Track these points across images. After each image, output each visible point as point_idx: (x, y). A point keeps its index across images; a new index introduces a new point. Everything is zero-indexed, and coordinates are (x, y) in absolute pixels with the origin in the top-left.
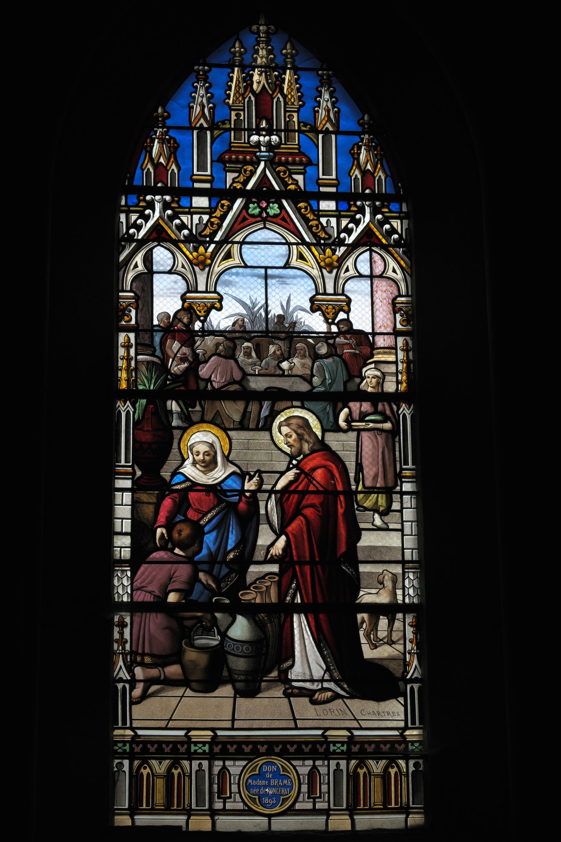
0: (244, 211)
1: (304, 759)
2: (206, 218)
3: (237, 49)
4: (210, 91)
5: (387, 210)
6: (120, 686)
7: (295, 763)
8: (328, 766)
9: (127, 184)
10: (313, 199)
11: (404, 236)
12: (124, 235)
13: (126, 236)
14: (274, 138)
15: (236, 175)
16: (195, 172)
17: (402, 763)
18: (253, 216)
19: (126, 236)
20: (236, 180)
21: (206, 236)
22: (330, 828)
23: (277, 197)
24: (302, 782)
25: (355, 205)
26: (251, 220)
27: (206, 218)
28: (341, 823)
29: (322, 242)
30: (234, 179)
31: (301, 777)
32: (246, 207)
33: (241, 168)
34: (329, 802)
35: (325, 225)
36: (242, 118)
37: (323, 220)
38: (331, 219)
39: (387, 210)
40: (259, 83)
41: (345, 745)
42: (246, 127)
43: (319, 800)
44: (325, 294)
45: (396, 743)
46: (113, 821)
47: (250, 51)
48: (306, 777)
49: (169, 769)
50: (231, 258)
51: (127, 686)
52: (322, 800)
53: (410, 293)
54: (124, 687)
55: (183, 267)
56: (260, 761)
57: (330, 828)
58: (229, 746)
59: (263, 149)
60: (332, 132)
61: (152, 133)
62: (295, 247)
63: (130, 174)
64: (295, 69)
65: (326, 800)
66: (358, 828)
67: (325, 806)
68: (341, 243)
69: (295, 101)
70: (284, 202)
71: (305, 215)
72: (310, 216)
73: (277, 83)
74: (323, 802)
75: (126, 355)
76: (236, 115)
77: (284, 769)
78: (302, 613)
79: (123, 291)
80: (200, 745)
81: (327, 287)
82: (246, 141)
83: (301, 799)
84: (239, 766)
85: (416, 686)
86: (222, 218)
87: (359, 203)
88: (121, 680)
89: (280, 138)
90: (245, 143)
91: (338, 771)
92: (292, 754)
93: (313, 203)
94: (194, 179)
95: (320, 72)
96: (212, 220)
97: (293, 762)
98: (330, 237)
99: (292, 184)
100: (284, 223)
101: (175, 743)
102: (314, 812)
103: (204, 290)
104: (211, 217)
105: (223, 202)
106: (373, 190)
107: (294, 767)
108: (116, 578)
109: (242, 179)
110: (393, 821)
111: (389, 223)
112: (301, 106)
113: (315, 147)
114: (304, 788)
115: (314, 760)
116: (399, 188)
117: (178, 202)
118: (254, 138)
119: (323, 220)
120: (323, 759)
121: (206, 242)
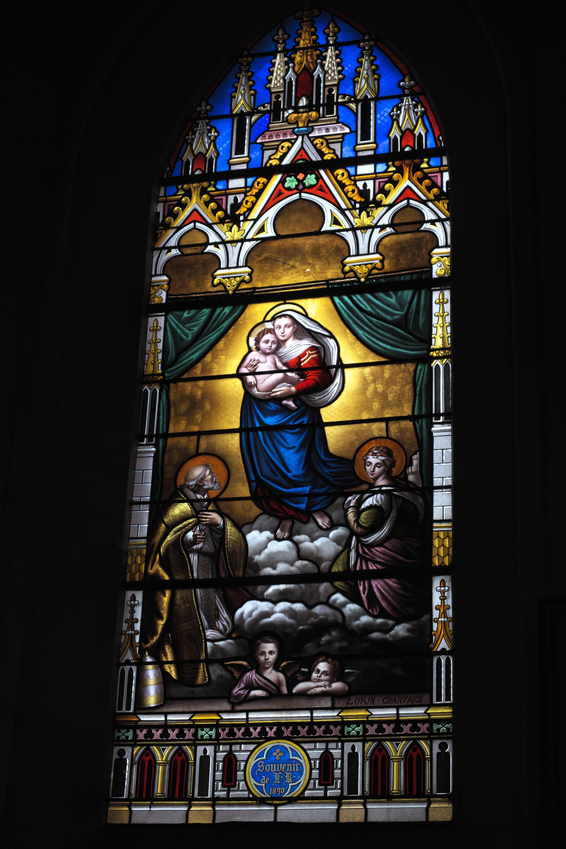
0: (281, 184)
1: (315, 742)
5: (213, 189)
7: (305, 746)
8: (342, 748)
9: (165, 176)
10: (350, 165)
11: (445, 189)
14: (314, 114)
18: (289, 189)
20: (272, 157)
22: (343, 819)
24: (313, 767)
28: (352, 812)
31: (312, 762)
32: (282, 181)
33: (278, 145)
38: (367, 182)
40: (301, 63)
45: (283, 726)
46: (168, 589)
48: (318, 761)
50: (264, 231)
51: (134, 669)
52: (334, 787)
57: (431, 819)
59: (301, 125)
60: (372, 99)
61: (195, 125)
63: (170, 167)
64: (337, 45)
66: (372, 818)
68: (378, 204)
69: (335, 75)
70: (322, 172)
71: (341, 181)
72: (346, 181)
73: (318, 61)
74: (335, 789)
79: (156, 275)
83: (311, 786)
86: (258, 196)
87: (185, 186)
88: (128, 663)
90: (283, 122)
93: (351, 170)
97: (303, 745)
100: (320, 193)
101: (327, 724)
102: (325, 799)
105: (259, 180)
107: (305, 750)
109: (278, 155)
110: (410, 810)
112: (340, 80)
113: (353, 115)
114: (316, 773)
116: (440, 141)
120: (337, 742)
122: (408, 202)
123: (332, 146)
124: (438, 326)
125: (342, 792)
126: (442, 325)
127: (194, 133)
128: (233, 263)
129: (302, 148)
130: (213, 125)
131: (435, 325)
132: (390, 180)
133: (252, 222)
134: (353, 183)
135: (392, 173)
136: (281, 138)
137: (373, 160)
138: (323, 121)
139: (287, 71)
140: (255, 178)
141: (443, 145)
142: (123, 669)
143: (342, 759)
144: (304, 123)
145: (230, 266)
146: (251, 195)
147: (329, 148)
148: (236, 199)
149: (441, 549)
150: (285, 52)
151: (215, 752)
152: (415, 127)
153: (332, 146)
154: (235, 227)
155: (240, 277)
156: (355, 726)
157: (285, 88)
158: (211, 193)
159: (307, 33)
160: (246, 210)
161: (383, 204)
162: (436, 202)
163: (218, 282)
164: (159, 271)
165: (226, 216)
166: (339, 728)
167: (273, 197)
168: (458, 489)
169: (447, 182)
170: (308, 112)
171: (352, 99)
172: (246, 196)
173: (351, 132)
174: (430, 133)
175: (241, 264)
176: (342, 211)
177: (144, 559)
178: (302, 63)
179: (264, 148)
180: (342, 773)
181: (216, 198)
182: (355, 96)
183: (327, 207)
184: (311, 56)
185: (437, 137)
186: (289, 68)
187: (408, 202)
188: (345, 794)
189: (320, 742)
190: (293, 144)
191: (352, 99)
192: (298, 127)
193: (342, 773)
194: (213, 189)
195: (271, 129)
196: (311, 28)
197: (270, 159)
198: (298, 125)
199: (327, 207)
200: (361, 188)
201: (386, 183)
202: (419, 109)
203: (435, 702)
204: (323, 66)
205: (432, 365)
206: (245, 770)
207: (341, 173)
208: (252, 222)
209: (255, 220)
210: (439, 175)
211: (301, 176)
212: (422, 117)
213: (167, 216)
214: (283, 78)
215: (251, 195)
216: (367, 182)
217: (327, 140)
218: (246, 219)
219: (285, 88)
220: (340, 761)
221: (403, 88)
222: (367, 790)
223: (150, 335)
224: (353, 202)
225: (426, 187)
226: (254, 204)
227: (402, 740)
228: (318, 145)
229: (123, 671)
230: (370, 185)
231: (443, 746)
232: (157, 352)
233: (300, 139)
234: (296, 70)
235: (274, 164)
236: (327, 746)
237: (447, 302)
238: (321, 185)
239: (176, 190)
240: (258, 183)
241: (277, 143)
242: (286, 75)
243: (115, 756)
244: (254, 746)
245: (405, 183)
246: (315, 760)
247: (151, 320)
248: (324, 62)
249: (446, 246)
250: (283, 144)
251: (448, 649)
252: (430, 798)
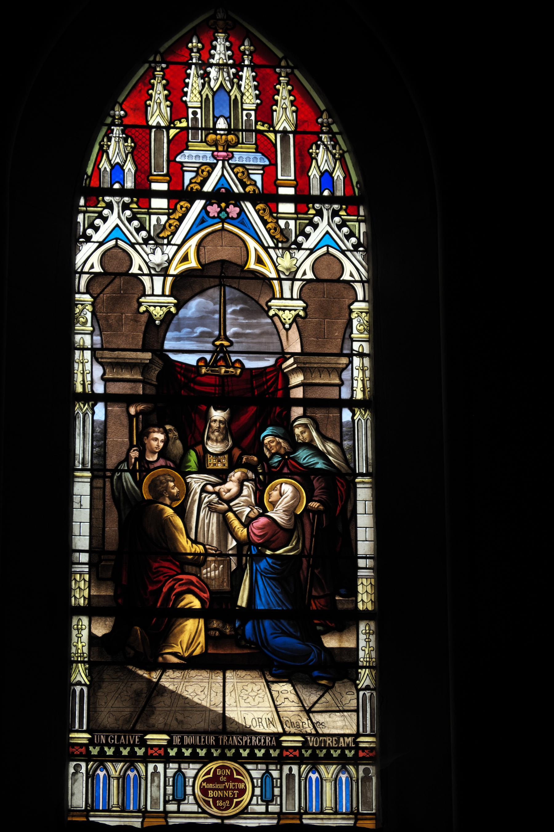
1: (257, 764)
2: (164, 219)
3: (194, 44)
6: (78, 689)
7: (249, 767)
8: (281, 771)
16: (280, 177)
17: (351, 768)
20: (193, 181)
21: (163, 238)
23: (237, 199)
24: (256, 785)
25: (313, 208)
26: (211, 221)
27: (164, 219)
34: (281, 805)
38: (289, 221)
42: (244, 128)
44: (282, 298)
47: (208, 47)
48: (259, 780)
50: (188, 260)
53: (367, 299)
54: (82, 690)
56: (213, 766)
58: (241, 751)
59: (220, 148)
65: (279, 803)
68: (299, 247)
74: (275, 805)
76: (247, 115)
77: (239, 773)
78: (202, 618)
80: (291, 751)
82: (204, 140)
83: (254, 801)
86: (181, 220)
88: (79, 683)
90: (201, 142)
91: (290, 776)
92: (245, 758)
96: (171, 222)
99: (250, 184)
104: (169, 219)
105: (182, 203)
106: (332, 192)
108: (74, 581)
109: (199, 179)
114: (258, 791)
115: (267, 764)
119: (282, 223)
120: (276, 764)
122: (117, 242)
124: (359, 379)
126: (82, 372)
128: (287, 294)
129: (223, 175)
130: (130, 134)
131: (356, 378)
133: (176, 247)
134: (275, 221)
136: (201, 161)
138: (241, 148)
140: (178, 201)
142: (74, 689)
143: (281, 778)
144: (224, 148)
145: (155, 293)
148: (158, 220)
151: (165, 769)
154: (158, 250)
155: (166, 307)
156: (293, 750)
157: (202, 104)
160: (169, 233)
161: (303, 247)
162: (144, 246)
163: (145, 309)
164: (82, 288)
165: (150, 238)
167: (197, 222)
173: (271, 164)
175: (167, 293)
176: (266, 249)
177: (87, 584)
178: (218, 79)
179: (184, 168)
180: (281, 791)
181: (138, 216)
183: (252, 244)
187: (117, 242)
189: (261, 763)
190: (213, 169)
193: (281, 791)
194: (136, 207)
196: (226, 42)
199: (252, 244)
200: (283, 226)
201: (97, 218)
202: (314, 151)
204: (239, 87)
206: (193, 786)
209: (180, 246)
210: (147, 217)
212: (132, 153)
213: (88, 228)
214: (200, 93)
215: (174, 219)
216: (289, 221)
218: (169, 243)
219: (202, 104)
220: (279, 780)
222: (302, 806)
224: (275, 241)
225: (135, 229)
229: (74, 691)
231: (366, 771)
232: (85, 373)
233: (220, 163)
234: (212, 86)
236: (267, 767)
238: (203, 217)
239: (307, 209)
242: (202, 90)
246: (257, 779)
248: (240, 82)
249: (364, 301)
250: (203, 168)
251: (372, 687)
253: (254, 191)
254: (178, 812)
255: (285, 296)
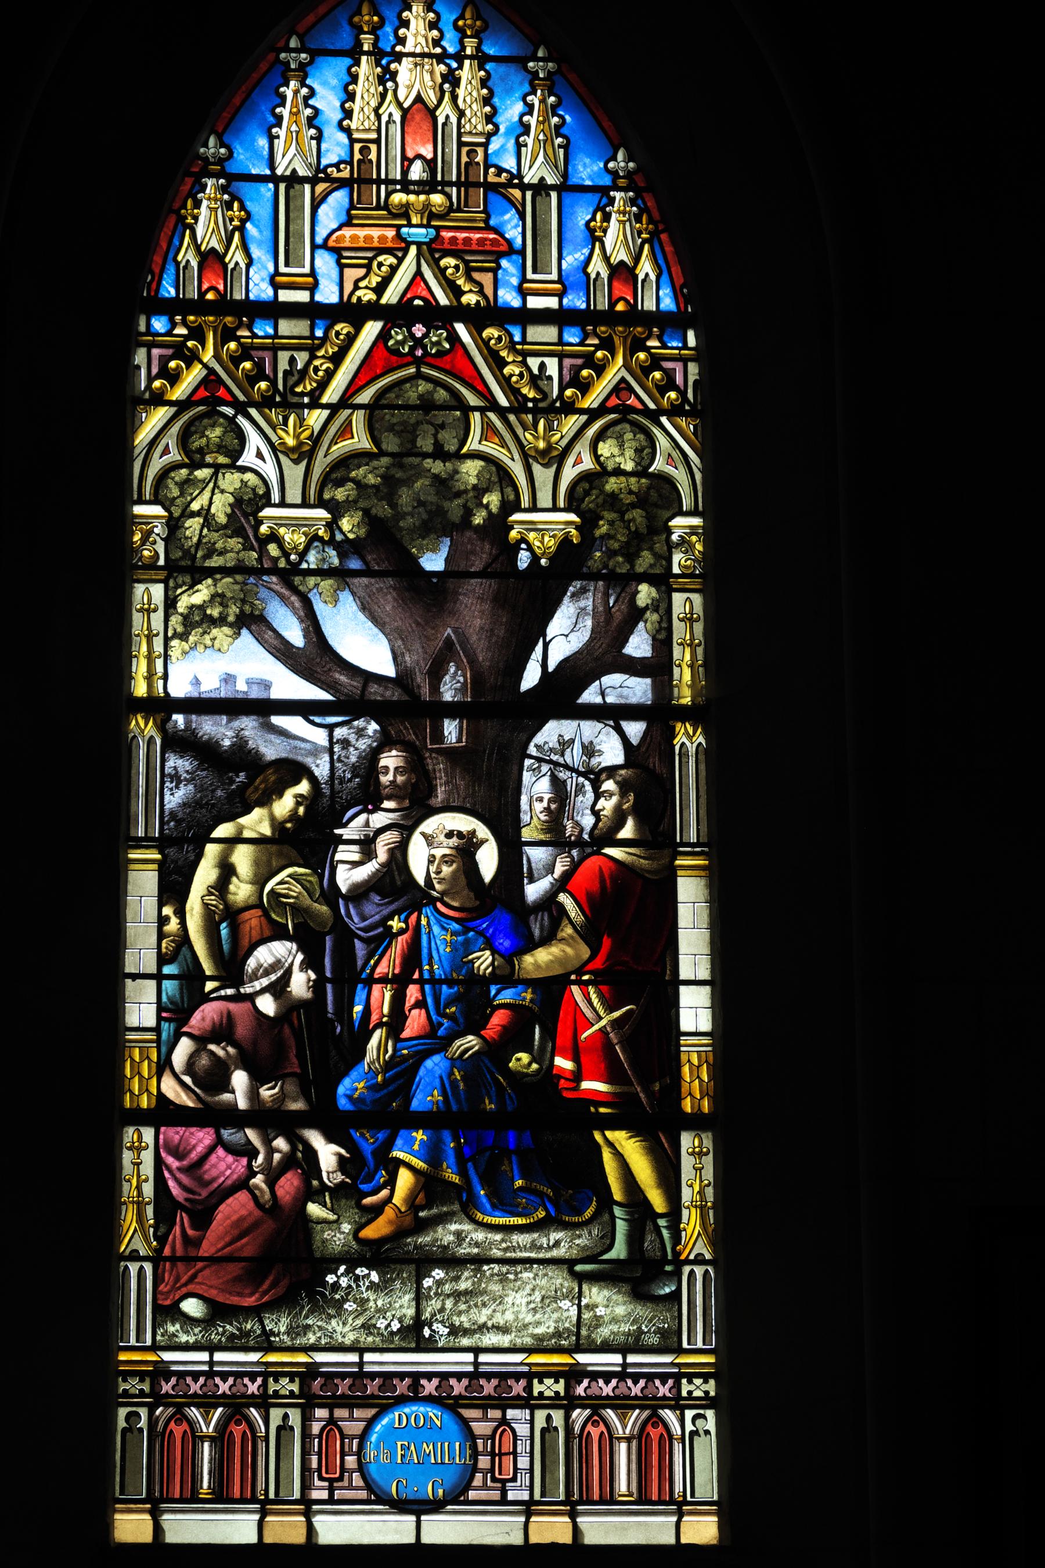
2: (301, 358)
4: (311, 102)
5: (247, 334)
10: (514, 323)
11: (690, 395)
12: (555, 401)
13: (558, 404)
14: (437, 199)
15: (362, 272)
19: (558, 404)
20: (362, 284)
27: (301, 358)
28: (552, 1529)
29: (530, 405)
30: (357, 282)
32: (383, 336)
33: (371, 260)
35: (536, 371)
36: (373, 156)
37: (534, 363)
39: (247, 334)
41: (297, 1380)
43: (340, 1484)
44: (283, 504)
46: (107, 1527)
49: (223, 1426)
51: (148, 1267)
55: (166, 451)
56: (420, 1409)
60: (553, 187)
61: (197, 187)
62: (477, 415)
64: (481, 59)
67: (525, 1496)
68: (569, 408)
75: (688, 637)
79: (141, 501)
81: (539, 495)
84: (492, 1420)
85: (699, 1271)
86: (337, 359)
88: (134, 1256)
89: (449, 197)
90: (378, 208)
94: (527, 289)
95: (531, 64)
96: (317, 363)
98: (545, 396)
103: (550, 506)
105: (338, 327)
109: (375, 280)
111: (660, 368)
117: (250, 328)
118: (398, 198)
119: (534, 363)
121: (303, 406)
123: (476, 276)
125: (532, 1494)
127: (197, 204)
128: (544, 499)
132: (589, 360)
135: (592, 349)
137: (560, 318)
139: (383, 96)
141: (690, 310)
142: (126, 1267)
146: (366, 287)
147: (470, 279)
148: (292, 361)
149: (695, 1083)
150: (377, 54)
152: (637, 259)
153: (476, 276)
158: (242, 340)
159: (421, 22)
166: (523, 1383)
168: (724, 986)
169: (695, 382)
170: (428, 193)
171: (516, 181)
172: (313, 357)
174: (665, 278)
182: (520, 176)
184: (432, 73)
185: (678, 288)
186: (386, 90)
188: (537, 1496)
190: (400, 260)
191: (516, 181)
192: (410, 225)
195: (355, 222)
197: (356, 287)
198: (409, 220)
203: (685, 1345)
204: (454, 98)
205: (675, 742)
207: (496, 336)
208: (326, 413)
211: (419, 330)
215: (366, 287)
217: (466, 263)
218: (315, 404)
221: (614, 174)
223: (137, 619)
225: (657, 386)
226: (330, 375)
227: (633, 1408)
228: (450, 271)
230: (552, 366)
234: (401, 99)
235: (365, 299)
237: (698, 620)
240: (338, 334)
241: (370, 254)
242: (380, 105)
243: (122, 1423)
244: (373, 1412)
245: (615, 372)
247: (139, 589)
250: (380, 259)
251: (708, 1256)
252: (680, 1507)
253: (478, 302)
254: (331, 1501)
255: (541, 504)
